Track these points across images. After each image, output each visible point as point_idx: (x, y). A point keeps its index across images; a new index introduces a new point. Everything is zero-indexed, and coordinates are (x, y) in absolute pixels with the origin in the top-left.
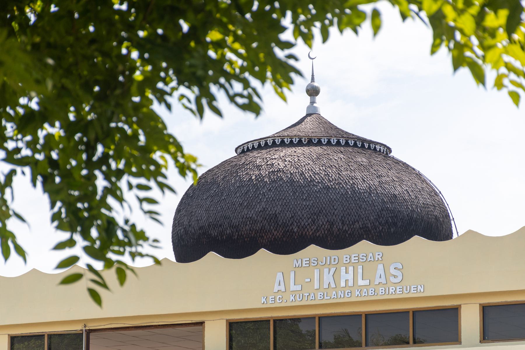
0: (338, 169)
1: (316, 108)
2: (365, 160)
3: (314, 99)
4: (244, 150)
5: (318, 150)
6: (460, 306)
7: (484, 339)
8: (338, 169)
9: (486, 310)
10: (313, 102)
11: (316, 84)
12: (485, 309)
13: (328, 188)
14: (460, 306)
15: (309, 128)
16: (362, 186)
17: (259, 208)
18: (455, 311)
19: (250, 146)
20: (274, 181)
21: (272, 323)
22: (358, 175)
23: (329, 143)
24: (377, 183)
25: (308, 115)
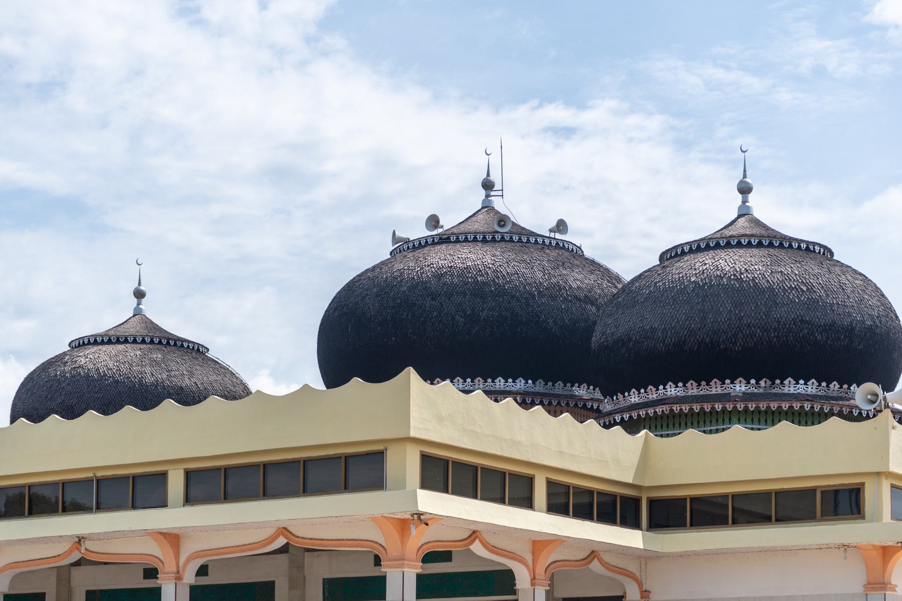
0: (131, 365)
1: (141, 309)
2: (160, 356)
3: (747, 198)
4: (80, 344)
5: (120, 347)
6: (167, 471)
7: (859, 489)
8: (131, 365)
9: (189, 475)
10: (744, 201)
11: (142, 288)
12: (188, 474)
13: (117, 382)
14: (167, 471)
15: (134, 329)
16: (149, 379)
17: (59, 400)
18: (163, 475)
19: (99, 339)
20: (74, 376)
21: (773, 495)
22: (148, 370)
23: (152, 342)
24: (164, 376)
25: (740, 216)
